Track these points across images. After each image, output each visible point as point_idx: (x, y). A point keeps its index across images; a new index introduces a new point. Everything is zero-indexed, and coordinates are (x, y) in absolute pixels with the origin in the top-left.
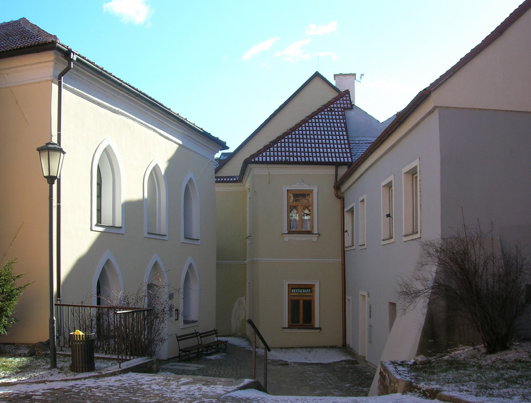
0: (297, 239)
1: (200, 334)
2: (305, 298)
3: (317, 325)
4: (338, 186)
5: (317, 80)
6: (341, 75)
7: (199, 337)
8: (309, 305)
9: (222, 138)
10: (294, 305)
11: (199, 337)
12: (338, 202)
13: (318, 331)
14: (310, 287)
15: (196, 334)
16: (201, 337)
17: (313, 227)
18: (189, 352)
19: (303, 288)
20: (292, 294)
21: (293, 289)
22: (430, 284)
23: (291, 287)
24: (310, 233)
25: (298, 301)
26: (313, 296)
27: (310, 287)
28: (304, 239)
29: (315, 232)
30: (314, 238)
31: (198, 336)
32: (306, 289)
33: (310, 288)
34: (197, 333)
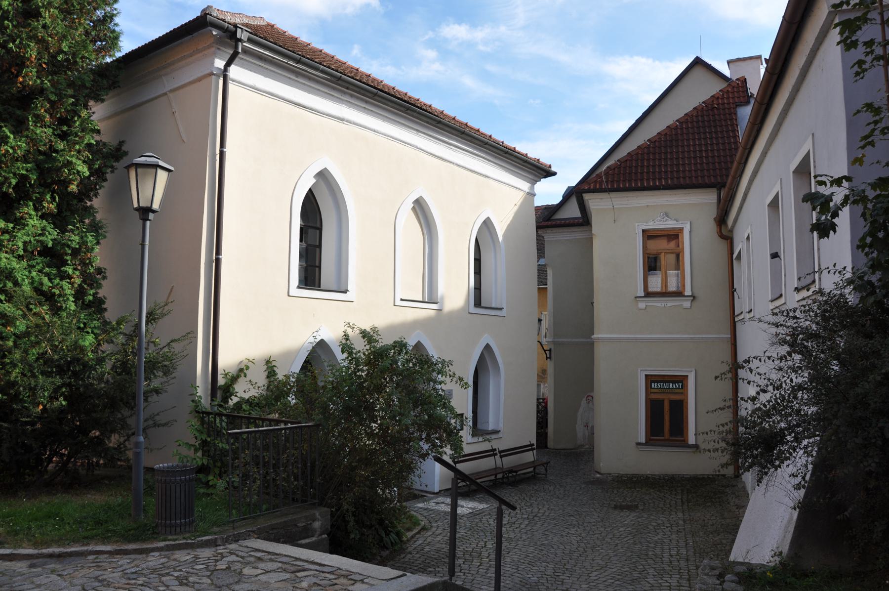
0: (659, 305)
1: (500, 452)
2: (673, 397)
3: (692, 440)
4: (721, 219)
5: (698, 71)
6: (739, 60)
7: (498, 457)
8: (679, 408)
9: (545, 160)
10: (654, 408)
11: (498, 457)
12: (723, 246)
13: (694, 449)
14: (682, 380)
15: (492, 453)
16: (501, 457)
17: (684, 286)
18: (516, 472)
19: (669, 382)
20: (653, 391)
21: (654, 382)
22: (317, 341)
23: (650, 379)
24: (679, 294)
25: (662, 402)
26: (685, 394)
27: (682, 380)
28: (670, 304)
29: (688, 292)
30: (687, 304)
31: (496, 454)
32: (674, 382)
33: (681, 382)
34: (495, 450)
